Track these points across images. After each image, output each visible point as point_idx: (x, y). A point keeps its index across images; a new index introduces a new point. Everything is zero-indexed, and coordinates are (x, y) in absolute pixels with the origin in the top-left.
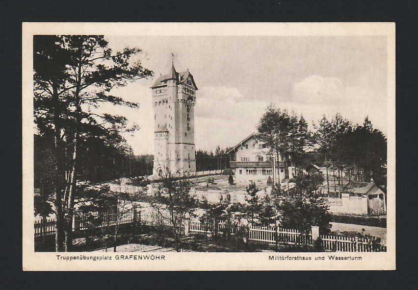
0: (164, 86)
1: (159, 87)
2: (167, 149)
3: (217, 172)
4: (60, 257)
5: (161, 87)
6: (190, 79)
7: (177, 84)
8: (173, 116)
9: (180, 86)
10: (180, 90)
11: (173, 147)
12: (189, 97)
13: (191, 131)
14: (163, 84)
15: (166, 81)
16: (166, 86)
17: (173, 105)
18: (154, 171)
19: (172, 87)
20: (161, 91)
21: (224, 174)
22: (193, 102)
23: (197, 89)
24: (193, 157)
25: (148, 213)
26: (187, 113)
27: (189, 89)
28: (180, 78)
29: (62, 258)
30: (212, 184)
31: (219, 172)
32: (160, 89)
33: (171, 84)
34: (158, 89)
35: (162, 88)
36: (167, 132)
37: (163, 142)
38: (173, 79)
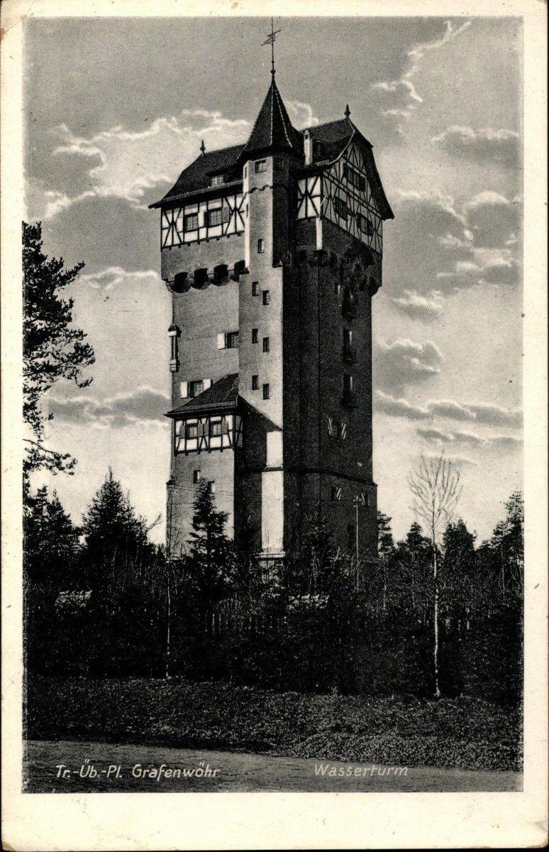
6: (356, 159)
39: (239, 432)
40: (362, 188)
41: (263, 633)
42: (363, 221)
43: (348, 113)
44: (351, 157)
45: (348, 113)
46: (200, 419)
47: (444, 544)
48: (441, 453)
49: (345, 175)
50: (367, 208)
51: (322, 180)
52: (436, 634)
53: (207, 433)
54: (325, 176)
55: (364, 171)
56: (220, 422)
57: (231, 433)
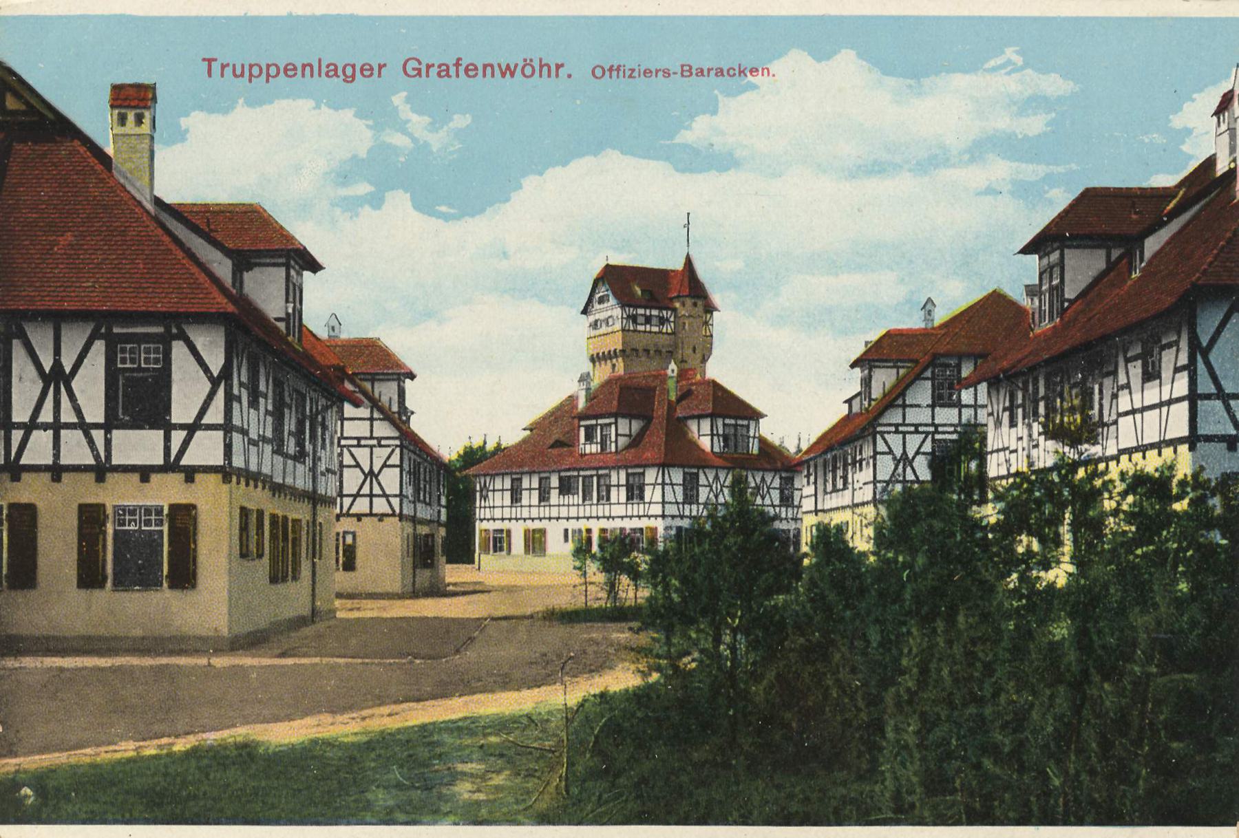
4: (216, 67)
29: (228, 71)
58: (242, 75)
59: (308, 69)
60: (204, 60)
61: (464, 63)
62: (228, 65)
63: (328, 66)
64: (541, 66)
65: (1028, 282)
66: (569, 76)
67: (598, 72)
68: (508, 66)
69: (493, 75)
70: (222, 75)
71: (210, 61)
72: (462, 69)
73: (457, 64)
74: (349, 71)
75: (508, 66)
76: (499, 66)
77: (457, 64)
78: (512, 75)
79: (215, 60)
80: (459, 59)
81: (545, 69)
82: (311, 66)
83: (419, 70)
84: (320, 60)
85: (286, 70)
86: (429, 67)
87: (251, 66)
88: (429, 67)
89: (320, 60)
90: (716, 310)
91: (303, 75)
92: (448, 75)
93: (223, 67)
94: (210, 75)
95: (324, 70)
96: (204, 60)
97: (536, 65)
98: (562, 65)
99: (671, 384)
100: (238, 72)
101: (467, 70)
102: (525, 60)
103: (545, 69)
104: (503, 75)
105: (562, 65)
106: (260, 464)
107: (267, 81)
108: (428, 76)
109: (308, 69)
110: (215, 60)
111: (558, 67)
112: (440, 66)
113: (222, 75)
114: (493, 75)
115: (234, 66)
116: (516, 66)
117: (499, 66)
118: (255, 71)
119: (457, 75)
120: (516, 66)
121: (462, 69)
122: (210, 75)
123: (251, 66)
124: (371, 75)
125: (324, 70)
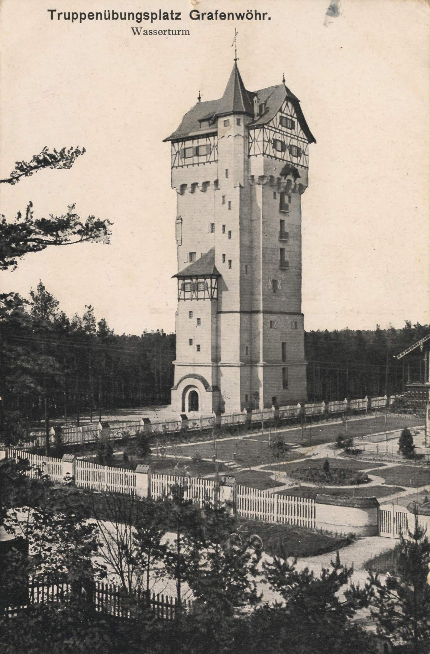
0: (207, 136)
1: (193, 138)
2: (216, 331)
3: (374, 404)
4: (55, 14)
5: (198, 137)
6: (289, 109)
7: (248, 128)
8: (235, 226)
9: (256, 134)
10: (257, 148)
11: (231, 326)
12: (287, 166)
13: (292, 270)
14: (205, 129)
15: (213, 119)
16: (215, 134)
17: (234, 196)
18: (176, 395)
19: (231, 139)
20: (197, 148)
21: (394, 409)
22: (298, 181)
23: (311, 139)
24: (297, 350)
25: (208, 281)
26: (278, 217)
27: (288, 141)
28: (256, 110)
29: (62, 16)
30: (348, 451)
31: (380, 402)
32: (196, 143)
33: (230, 131)
34: (189, 144)
35: (202, 141)
36: (218, 276)
37: (204, 308)
38: (234, 113)
39: (214, 288)
40: (293, 128)
41: (412, 588)
42: (294, 149)
43: (284, 81)
44: (286, 110)
45: (284, 81)
46: (205, 279)
47: (415, 449)
48: (255, 316)
49: (281, 123)
50: (297, 139)
51: (263, 131)
52: (293, 462)
53: (196, 288)
54: (266, 128)
55: (295, 116)
56: (203, 282)
57: (210, 290)
58: (69, 18)
59: (99, 15)
60: (49, 10)
61: (219, 12)
62: (62, 13)
63: (164, 14)
64: (256, 15)
65: (328, 330)
66: (270, 19)
67: (194, 15)
68: (240, 14)
69: (233, 19)
70: (59, 19)
71: (52, 11)
72: (218, 15)
73: (216, 14)
74: (139, 16)
75: (240, 14)
76: (236, 14)
77: (216, 14)
78: (242, 18)
79: (55, 11)
80: (217, 11)
81: (258, 16)
82: (101, 14)
83: (199, 16)
84: (160, 11)
85: (89, 16)
86: (203, 14)
87: (73, 14)
88: (203, 14)
89: (160, 11)
90: (227, 289)
91: (97, 19)
92: (212, 18)
93: (59, 14)
94: (52, 18)
95: (162, 16)
96: (49, 10)
97: (253, 13)
98: (266, 13)
99: (350, 448)
100: (67, 17)
101: (220, 16)
102: (248, 11)
103: (258, 16)
104: (238, 18)
105: (266, 13)
106: (126, 527)
107: (152, 22)
108: (203, 19)
109: (99, 15)
110: (55, 11)
111: (264, 14)
112: (208, 14)
113: (59, 19)
114: (233, 19)
115: (65, 13)
116: (244, 14)
117: (236, 14)
118: (75, 16)
119: (216, 19)
120: (244, 14)
121: (218, 15)
122: (52, 18)
123: (73, 14)
124: (93, 18)
125: (162, 16)
